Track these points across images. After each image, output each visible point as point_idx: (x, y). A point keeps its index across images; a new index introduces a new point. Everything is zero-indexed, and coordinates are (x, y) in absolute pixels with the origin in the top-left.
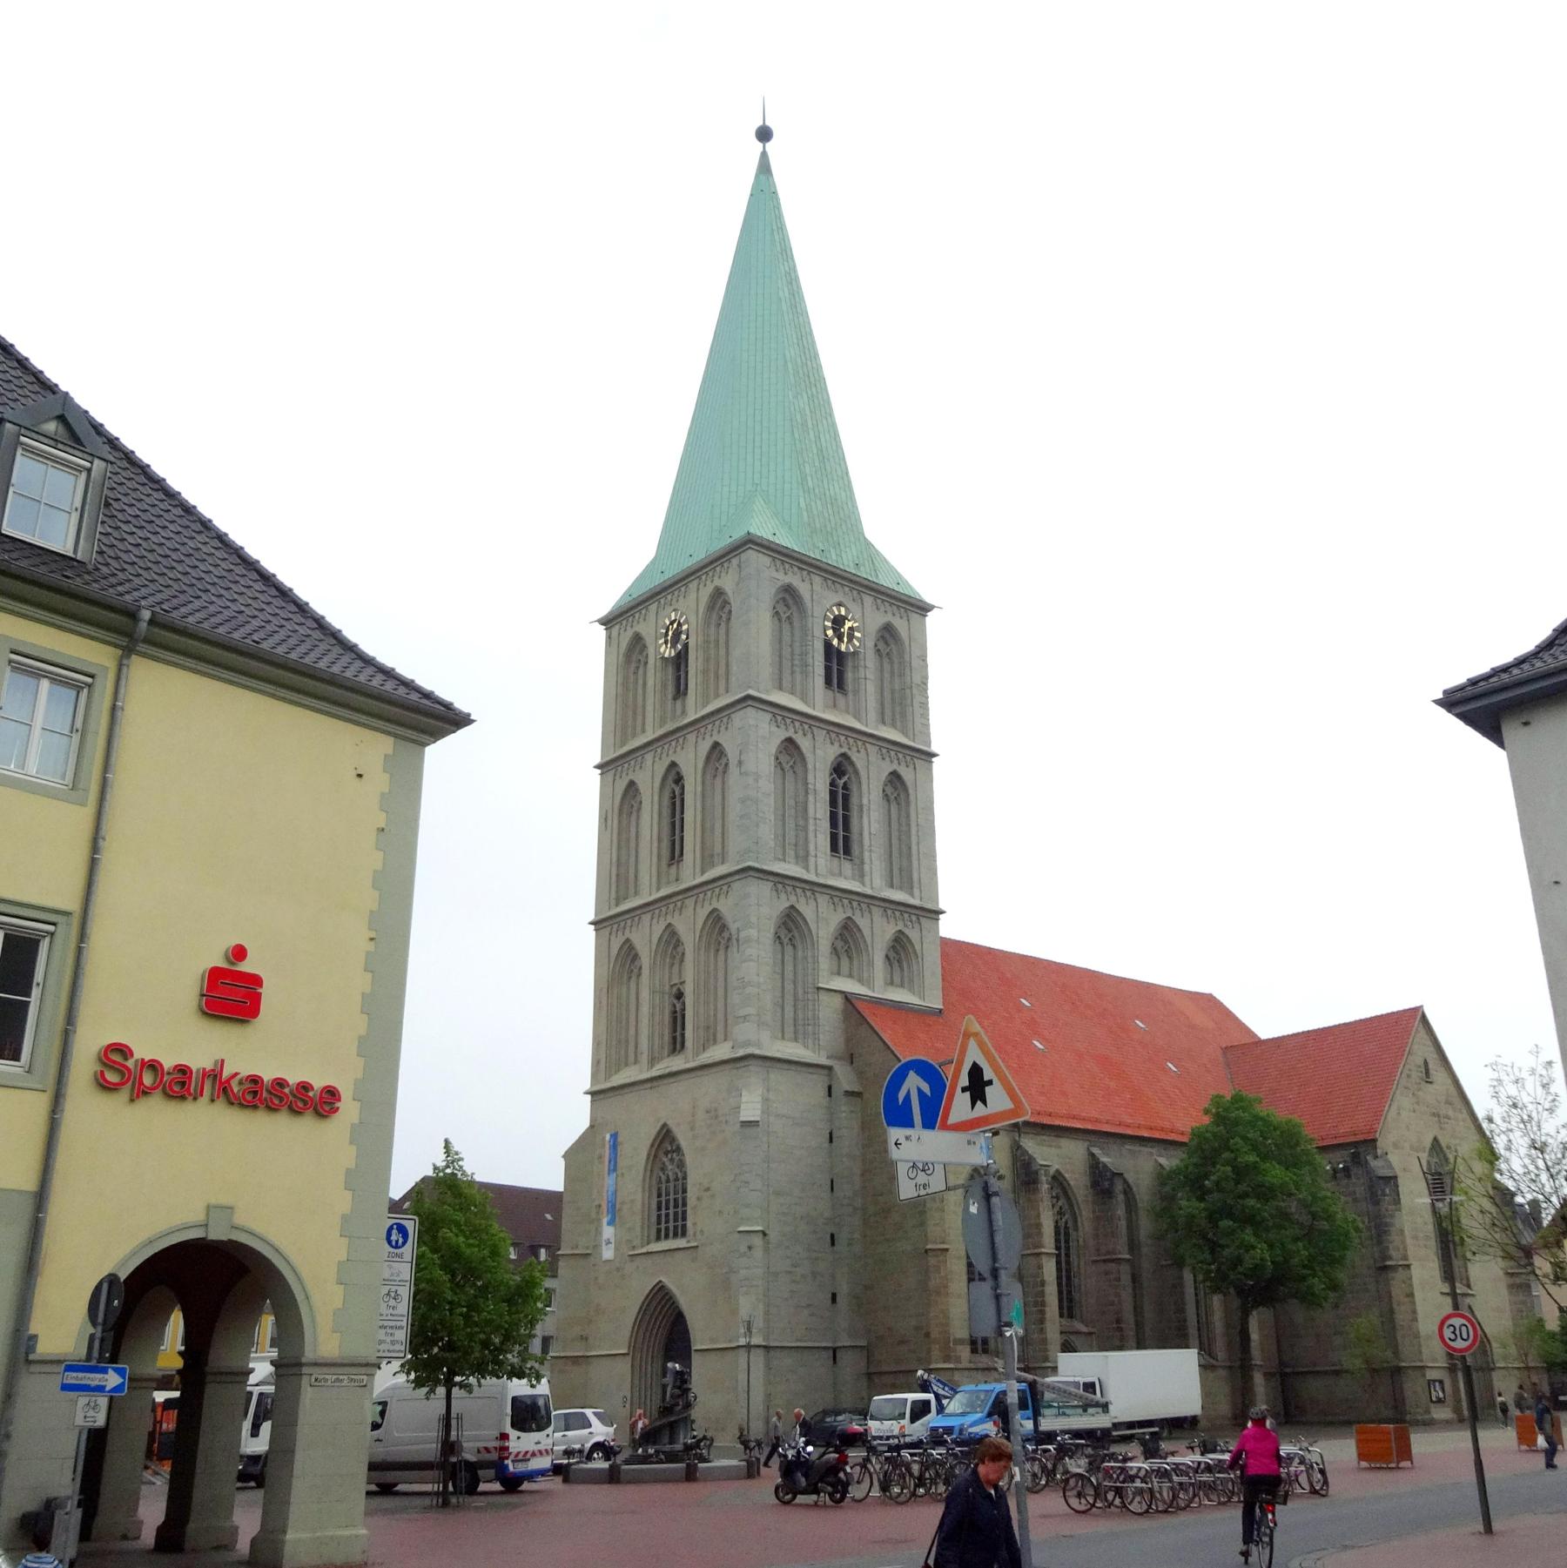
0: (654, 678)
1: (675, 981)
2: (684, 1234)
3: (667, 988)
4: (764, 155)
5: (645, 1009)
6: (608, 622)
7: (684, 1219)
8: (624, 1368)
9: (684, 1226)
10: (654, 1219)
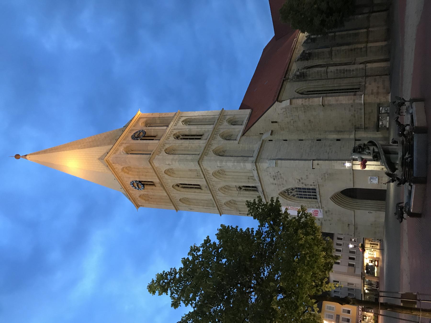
0: (148, 190)
1: (236, 189)
2: (315, 189)
3: (238, 192)
4: (22, 157)
5: (385, 278)
6: (138, 206)
7: (309, 189)
8: (358, 212)
9: (312, 189)
10: (310, 200)
